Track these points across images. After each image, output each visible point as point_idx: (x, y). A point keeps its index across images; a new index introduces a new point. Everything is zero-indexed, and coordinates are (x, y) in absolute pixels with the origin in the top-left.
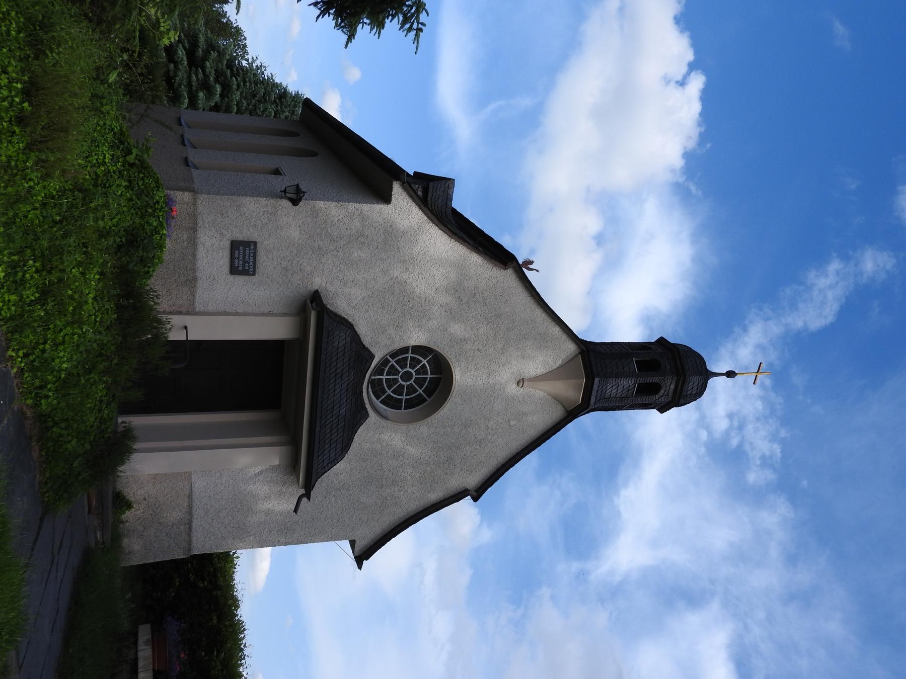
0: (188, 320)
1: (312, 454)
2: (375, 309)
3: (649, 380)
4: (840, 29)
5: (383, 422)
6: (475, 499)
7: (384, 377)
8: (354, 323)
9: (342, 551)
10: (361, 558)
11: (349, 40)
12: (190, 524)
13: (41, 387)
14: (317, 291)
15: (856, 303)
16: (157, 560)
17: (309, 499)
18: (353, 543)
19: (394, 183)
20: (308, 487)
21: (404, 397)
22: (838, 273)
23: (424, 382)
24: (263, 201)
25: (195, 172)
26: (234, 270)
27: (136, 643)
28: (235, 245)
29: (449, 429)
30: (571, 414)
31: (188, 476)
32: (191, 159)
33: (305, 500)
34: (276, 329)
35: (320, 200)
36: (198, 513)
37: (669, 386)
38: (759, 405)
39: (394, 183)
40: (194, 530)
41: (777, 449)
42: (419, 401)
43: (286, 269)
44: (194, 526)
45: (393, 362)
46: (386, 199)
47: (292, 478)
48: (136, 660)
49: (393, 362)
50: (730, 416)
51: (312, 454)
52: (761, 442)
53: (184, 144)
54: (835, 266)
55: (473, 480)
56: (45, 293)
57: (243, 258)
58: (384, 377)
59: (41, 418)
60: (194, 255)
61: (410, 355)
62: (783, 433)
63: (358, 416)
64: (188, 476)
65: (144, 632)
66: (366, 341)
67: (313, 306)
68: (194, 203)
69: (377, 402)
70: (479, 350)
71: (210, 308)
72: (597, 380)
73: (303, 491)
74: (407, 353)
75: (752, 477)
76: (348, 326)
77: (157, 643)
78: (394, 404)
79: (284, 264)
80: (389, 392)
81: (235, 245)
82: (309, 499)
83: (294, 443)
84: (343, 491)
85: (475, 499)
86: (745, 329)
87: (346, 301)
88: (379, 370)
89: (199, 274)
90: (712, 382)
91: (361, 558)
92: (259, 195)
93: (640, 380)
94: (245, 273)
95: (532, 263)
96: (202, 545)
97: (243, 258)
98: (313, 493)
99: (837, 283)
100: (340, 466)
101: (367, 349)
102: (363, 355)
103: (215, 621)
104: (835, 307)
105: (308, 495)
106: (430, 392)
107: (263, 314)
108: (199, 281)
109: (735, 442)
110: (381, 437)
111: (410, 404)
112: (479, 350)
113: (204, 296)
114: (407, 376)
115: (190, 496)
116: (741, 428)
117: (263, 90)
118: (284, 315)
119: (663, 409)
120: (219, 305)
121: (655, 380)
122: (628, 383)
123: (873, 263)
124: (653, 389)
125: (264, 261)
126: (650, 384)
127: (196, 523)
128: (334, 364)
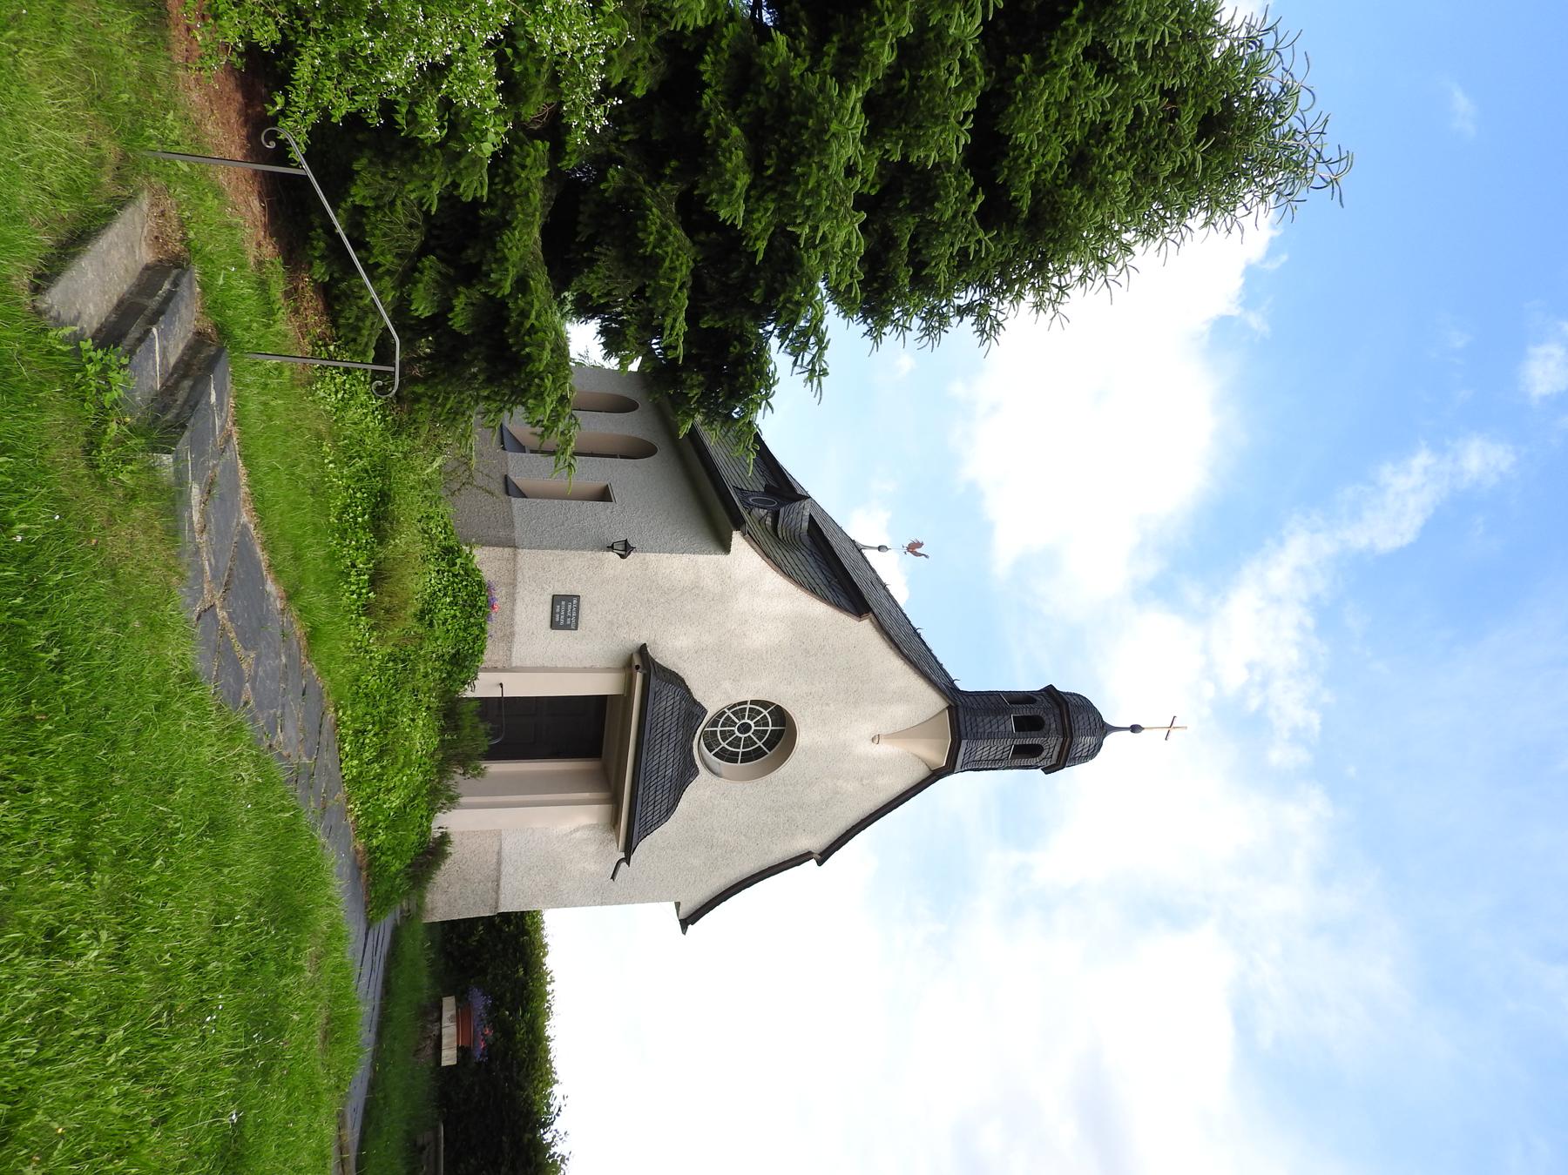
0: (503, 677)
1: (636, 813)
4: (1462, 102)
5: (715, 779)
6: (820, 863)
7: (719, 729)
9: (666, 915)
10: (685, 923)
12: (498, 881)
13: (373, 827)
14: (644, 646)
15: (1447, 520)
18: (678, 905)
20: (629, 849)
21: (741, 750)
22: (1426, 470)
23: (767, 736)
24: (588, 554)
25: (517, 502)
26: (554, 625)
27: (440, 1019)
28: (556, 599)
30: (935, 775)
31: (498, 834)
32: (516, 479)
34: (602, 684)
35: (652, 550)
36: (507, 869)
37: (1052, 744)
38: (1294, 654)
41: (1315, 719)
42: (758, 753)
43: (611, 623)
44: (502, 884)
45: (729, 713)
46: (725, 547)
47: (612, 836)
48: (440, 1037)
50: (1250, 667)
51: (636, 813)
52: (1293, 706)
53: (507, 493)
54: (1422, 459)
55: (817, 843)
56: (382, 753)
57: (564, 612)
58: (719, 729)
59: (370, 851)
60: (512, 610)
61: (748, 706)
62: (1327, 697)
63: (687, 772)
64: (498, 834)
65: (449, 1005)
66: (698, 696)
67: (641, 663)
68: (514, 559)
69: (710, 755)
71: (528, 663)
72: (964, 742)
73: (622, 855)
75: (1279, 756)
76: (676, 680)
77: (462, 1018)
78: (730, 757)
79: (609, 617)
80: (724, 744)
81: (556, 599)
83: (615, 801)
85: (820, 863)
86: (1281, 543)
87: (673, 650)
88: (714, 723)
89: (516, 629)
90: (1110, 741)
91: (685, 923)
93: (1018, 742)
94: (566, 627)
95: (920, 545)
96: (508, 905)
97: (564, 612)
99: (1424, 485)
100: (667, 827)
101: (699, 705)
102: (693, 710)
103: (521, 972)
104: (1418, 521)
105: (627, 860)
106: (771, 744)
107: (585, 670)
109: (1254, 703)
110: (714, 797)
111: (747, 758)
113: (523, 651)
114: (745, 728)
115: (499, 853)
116: (1264, 685)
117: (613, 223)
118: (608, 670)
119: (1048, 770)
120: (536, 662)
121: (1036, 741)
123: (1482, 459)
124: (1034, 751)
125: (589, 615)
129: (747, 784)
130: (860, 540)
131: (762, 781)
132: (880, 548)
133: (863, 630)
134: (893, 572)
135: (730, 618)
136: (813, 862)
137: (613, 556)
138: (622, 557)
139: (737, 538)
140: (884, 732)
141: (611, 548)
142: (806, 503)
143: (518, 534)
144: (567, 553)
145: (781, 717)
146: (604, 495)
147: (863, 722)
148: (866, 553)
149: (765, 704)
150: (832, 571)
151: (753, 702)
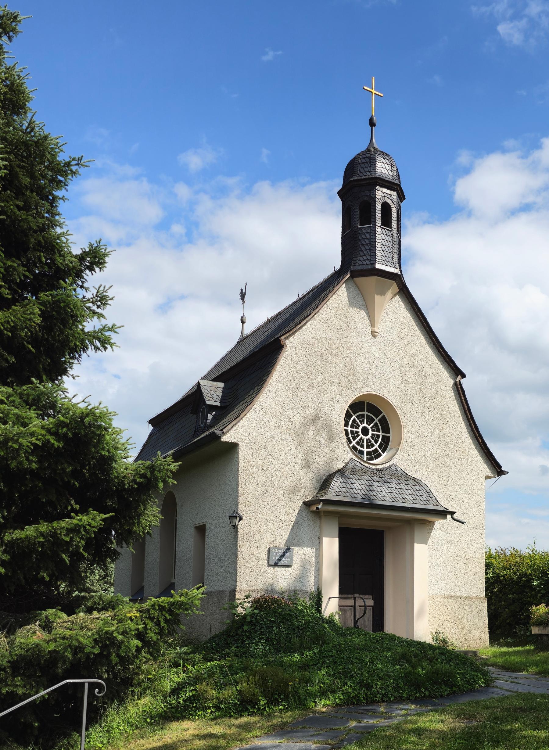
2: (317, 457)
3: (379, 214)
6: (463, 376)
7: (365, 450)
8: (327, 475)
11: (443, 513)
12: (464, 598)
16: (487, 621)
17: (454, 513)
19: (222, 440)
23: (372, 417)
24: (240, 542)
29: (409, 398)
33: (455, 516)
36: (458, 592)
39: (222, 440)
40: (468, 595)
44: (466, 595)
45: (354, 443)
46: (233, 447)
49: (354, 443)
61: (349, 429)
70: (348, 371)
72: (378, 266)
73: (449, 517)
74: (380, 447)
82: (454, 513)
84: (449, 485)
92: (236, 545)
93: (379, 223)
98: (451, 510)
105: (452, 513)
108: (297, 588)
111: (386, 429)
112: (348, 371)
115: (446, 597)
122: (381, 235)
126: (381, 214)
127: (463, 594)
128: (359, 491)
129: (404, 430)
130: (237, 337)
131: (403, 419)
132: (243, 322)
133: (294, 345)
134: (259, 314)
135: (277, 451)
136: (464, 382)
137: (241, 525)
138: (241, 519)
139: (225, 438)
140: (369, 328)
141: (235, 527)
142: (202, 382)
143: (227, 588)
144: (240, 556)
145: (356, 406)
146: (201, 530)
147: (354, 349)
148: (247, 332)
149: (348, 416)
150: (248, 369)
151: (346, 425)
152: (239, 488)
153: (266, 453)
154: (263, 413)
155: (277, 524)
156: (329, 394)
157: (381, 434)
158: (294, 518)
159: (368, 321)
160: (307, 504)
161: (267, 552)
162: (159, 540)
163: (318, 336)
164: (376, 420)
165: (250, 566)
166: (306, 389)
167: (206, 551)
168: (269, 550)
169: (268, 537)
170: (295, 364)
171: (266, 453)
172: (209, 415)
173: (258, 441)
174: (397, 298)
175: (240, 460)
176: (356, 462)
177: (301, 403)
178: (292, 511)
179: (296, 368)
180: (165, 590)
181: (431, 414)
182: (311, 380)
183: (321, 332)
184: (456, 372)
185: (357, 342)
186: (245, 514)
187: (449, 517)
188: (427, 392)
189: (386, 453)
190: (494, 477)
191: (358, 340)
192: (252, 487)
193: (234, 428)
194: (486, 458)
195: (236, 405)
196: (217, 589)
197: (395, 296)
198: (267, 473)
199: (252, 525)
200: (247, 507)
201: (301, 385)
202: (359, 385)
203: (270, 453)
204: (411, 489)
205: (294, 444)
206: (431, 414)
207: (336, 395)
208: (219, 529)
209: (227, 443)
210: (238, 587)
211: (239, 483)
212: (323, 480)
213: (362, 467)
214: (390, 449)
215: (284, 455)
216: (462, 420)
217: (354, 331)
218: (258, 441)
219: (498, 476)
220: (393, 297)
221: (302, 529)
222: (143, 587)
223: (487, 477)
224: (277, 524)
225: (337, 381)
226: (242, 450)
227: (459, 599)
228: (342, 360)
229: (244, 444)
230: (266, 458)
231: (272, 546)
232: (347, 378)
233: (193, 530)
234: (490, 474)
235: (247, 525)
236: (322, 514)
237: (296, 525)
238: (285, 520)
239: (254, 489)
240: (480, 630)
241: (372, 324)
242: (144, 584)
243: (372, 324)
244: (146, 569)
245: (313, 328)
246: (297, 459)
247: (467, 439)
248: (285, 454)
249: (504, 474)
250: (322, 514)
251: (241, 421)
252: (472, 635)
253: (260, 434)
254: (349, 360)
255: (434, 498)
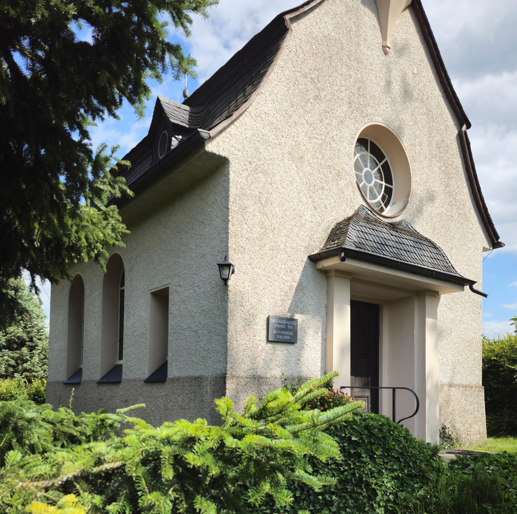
8: (335, 222)
11: (461, 282)
12: (465, 387)
17: (474, 282)
33: (475, 287)
46: (220, 164)
70: (359, 89)
73: (467, 288)
74: (383, 198)
82: (474, 282)
105: (471, 283)
112: (359, 89)
127: (465, 383)
140: (380, 40)
141: (225, 281)
152: (230, 226)
153: (264, 179)
154: (260, 121)
155: (277, 284)
156: (338, 114)
157: (383, 183)
158: (298, 277)
159: (379, 31)
160: (314, 259)
161: (265, 322)
162: (101, 314)
163: (326, 33)
164: (380, 165)
165: (244, 342)
166: (312, 100)
167: (170, 322)
168: (268, 319)
169: (267, 301)
170: (300, 63)
171: (264, 179)
172: (173, 139)
173: (255, 160)
174: (407, 13)
175: (231, 184)
176: (367, 210)
177: (307, 118)
178: (295, 267)
179: (301, 68)
180: (106, 374)
181: (437, 165)
182: (319, 90)
183: (329, 27)
184: (461, 119)
185: (367, 55)
186: (237, 266)
187: (467, 288)
188: (435, 138)
189: (389, 207)
190: (489, 250)
191: (369, 52)
192: (246, 227)
193: (223, 134)
194: (484, 227)
195: (214, 117)
196: (190, 374)
197: (405, 9)
198: (265, 209)
199: (246, 283)
200: (240, 256)
201: (306, 93)
202: (370, 111)
203: (270, 181)
204: (406, 255)
205: (298, 173)
206: (437, 165)
207: (345, 117)
208: (191, 291)
209: (213, 155)
210: (228, 372)
211: (230, 218)
212: (330, 229)
213: (374, 217)
214: (394, 204)
215: (286, 187)
216: (464, 179)
217: (365, 40)
218: (255, 160)
219: (493, 248)
220: (403, 11)
221: (307, 294)
222: (81, 369)
223: (485, 249)
224: (277, 284)
225: (347, 100)
226: (234, 169)
227: (461, 388)
228: (352, 73)
229: (236, 161)
230: (264, 187)
231: (271, 314)
232: (358, 99)
233: (148, 298)
234: (487, 246)
235: (240, 282)
236: (333, 274)
237: (300, 287)
238: (287, 279)
239: (249, 229)
240: (480, 424)
241: (384, 37)
242: (82, 366)
243: (384, 37)
244: (84, 348)
245: (321, 20)
246: (301, 195)
247: (468, 202)
248: (288, 185)
249: (501, 246)
250: (333, 274)
251: (232, 126)
252: (473, 430)
253: (257, 149)
254: (359, 75)
255: (450, 265)
